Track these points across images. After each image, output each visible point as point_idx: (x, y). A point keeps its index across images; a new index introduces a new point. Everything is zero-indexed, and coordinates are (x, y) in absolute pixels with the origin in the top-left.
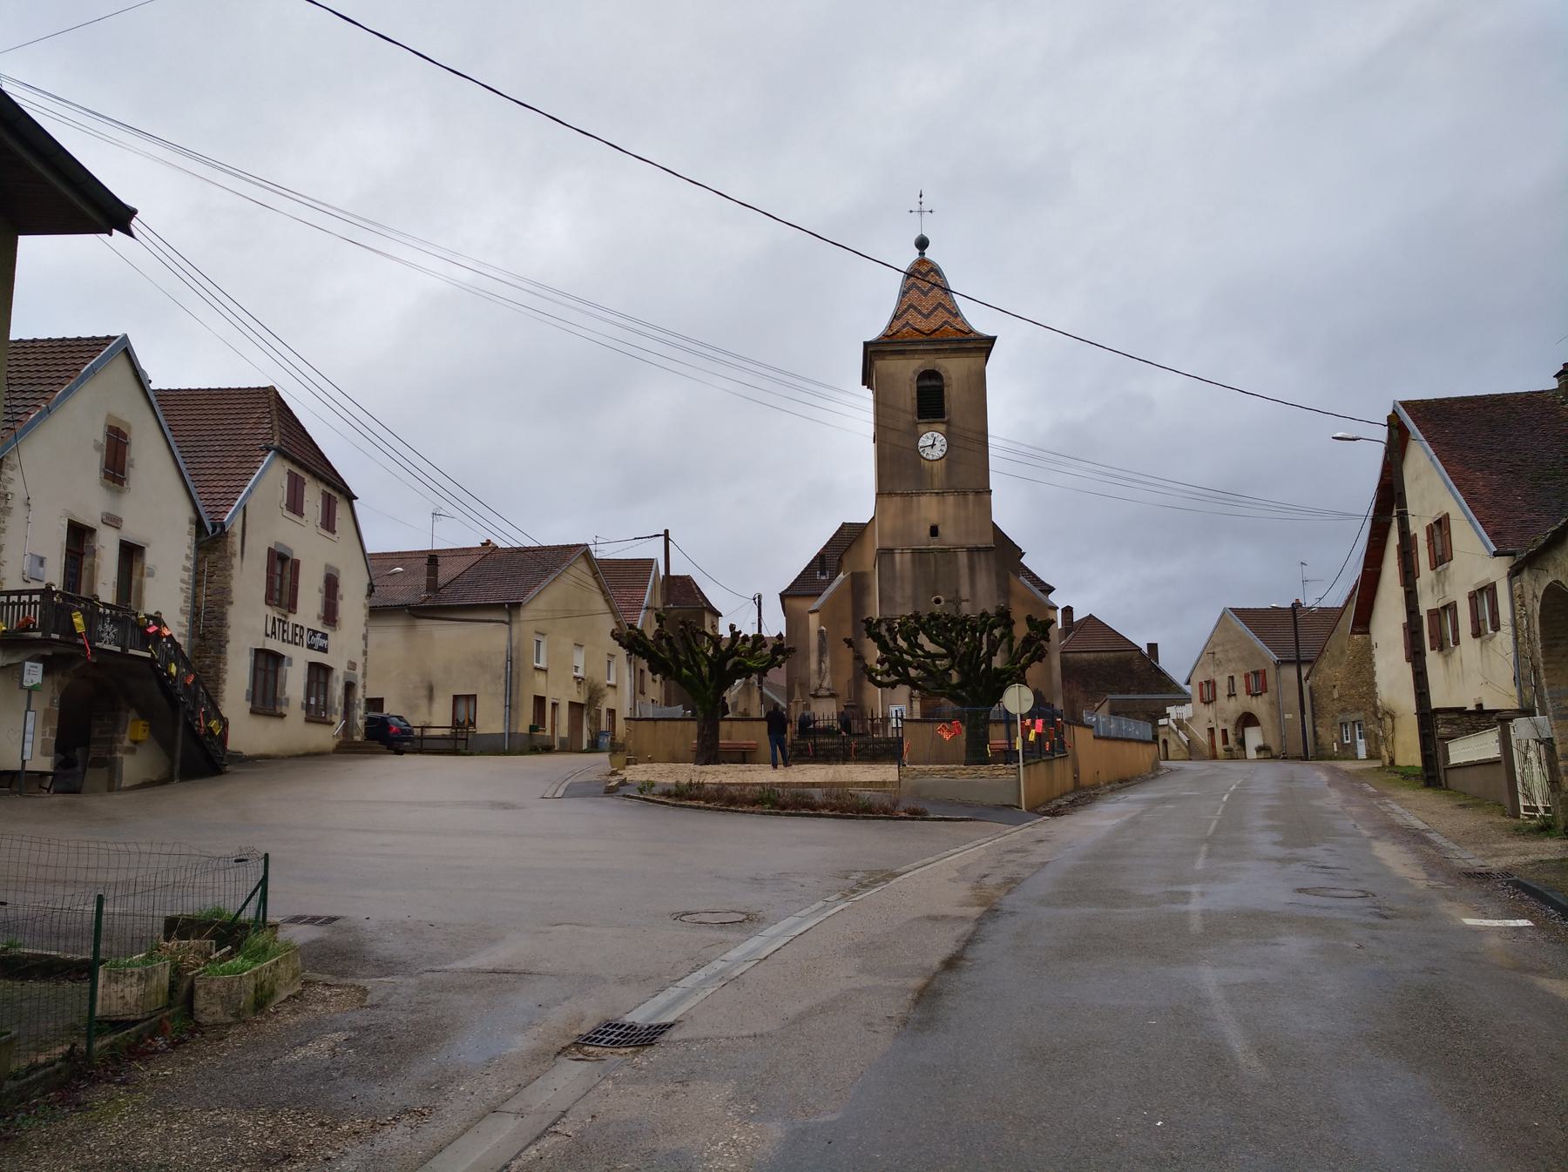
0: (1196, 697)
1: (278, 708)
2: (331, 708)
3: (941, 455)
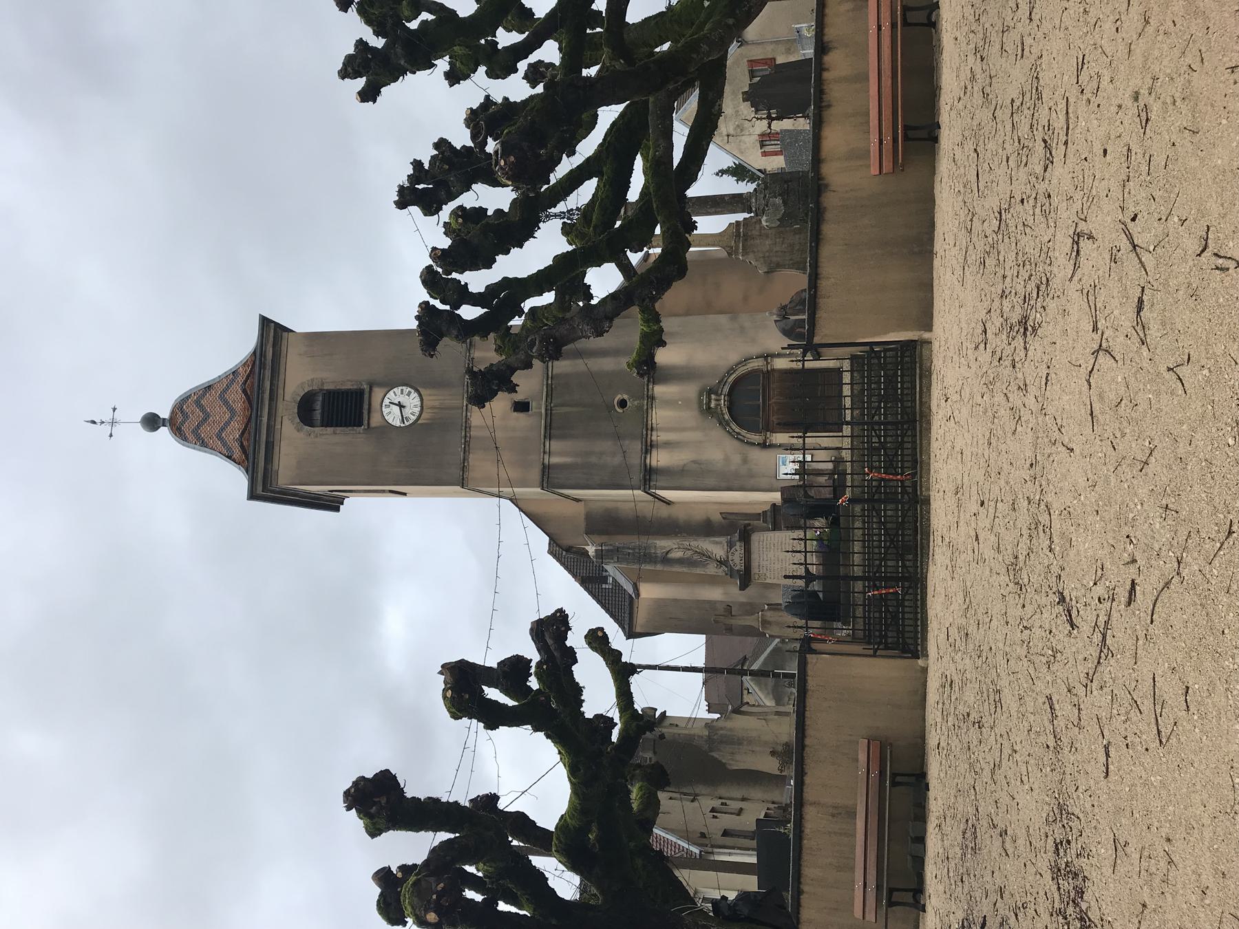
3: (416, 394)
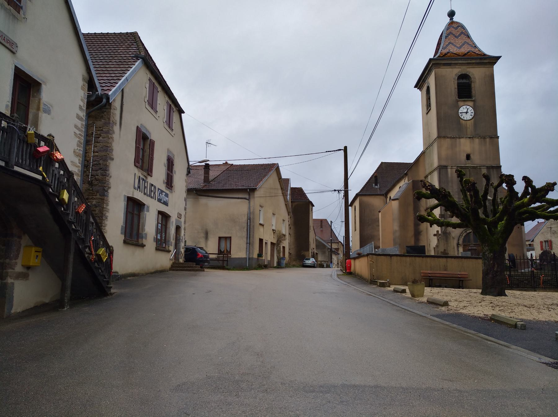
1: (140, 240)
2: (169, 241)
3: (471, 118)
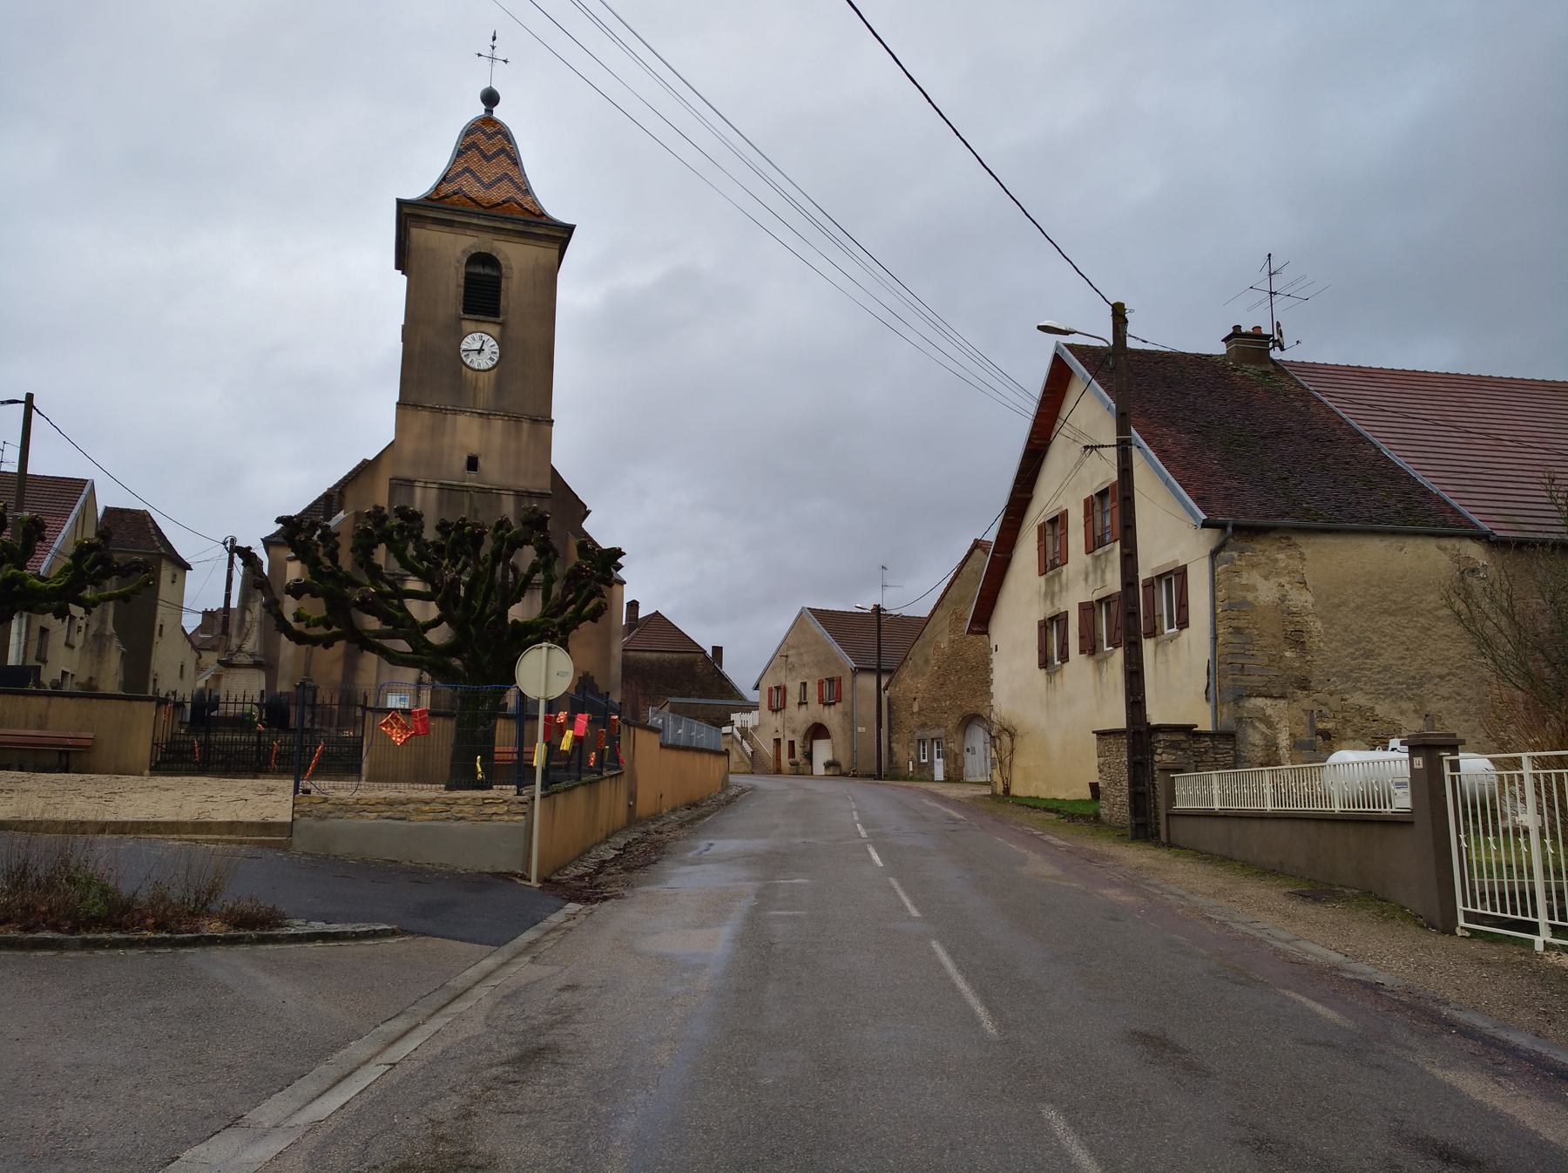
0: (764, 705)
3: (491, 366)
